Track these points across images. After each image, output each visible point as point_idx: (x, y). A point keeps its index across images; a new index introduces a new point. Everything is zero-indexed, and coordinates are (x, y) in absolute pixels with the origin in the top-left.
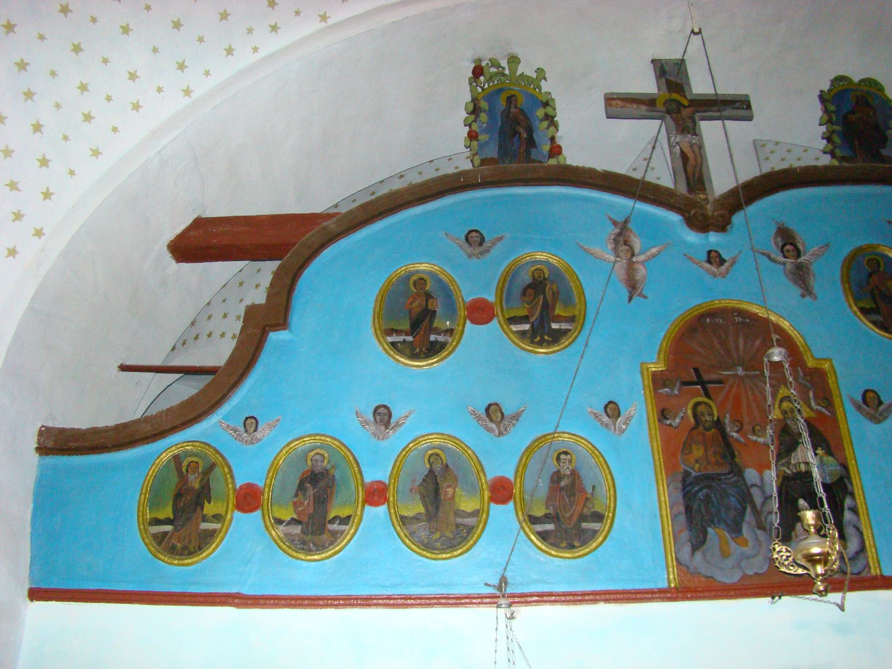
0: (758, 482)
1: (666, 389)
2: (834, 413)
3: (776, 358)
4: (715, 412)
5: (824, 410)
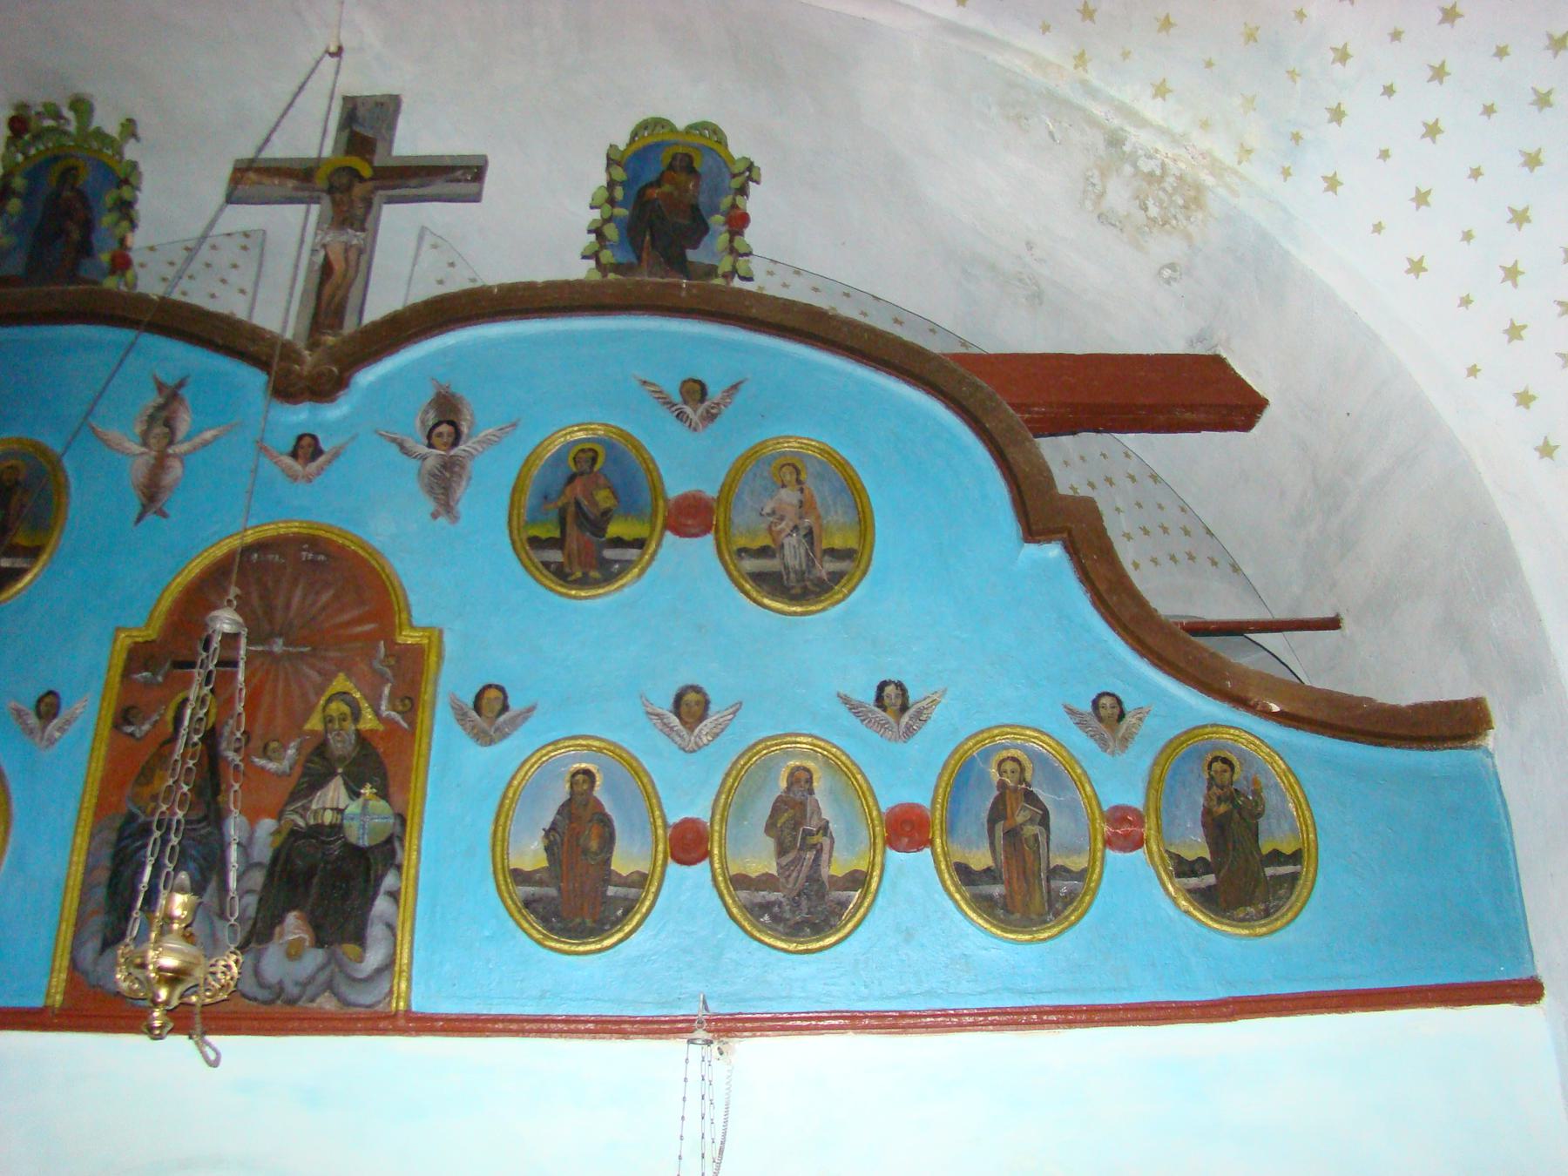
1: (144, 674)
3: (227, 628)
5: (398, 717)
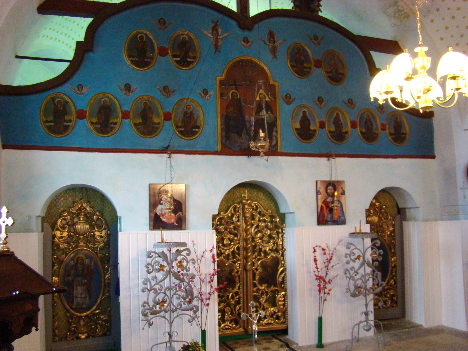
0: (248, 120)
2: (275, 100)
4: (238, 96)
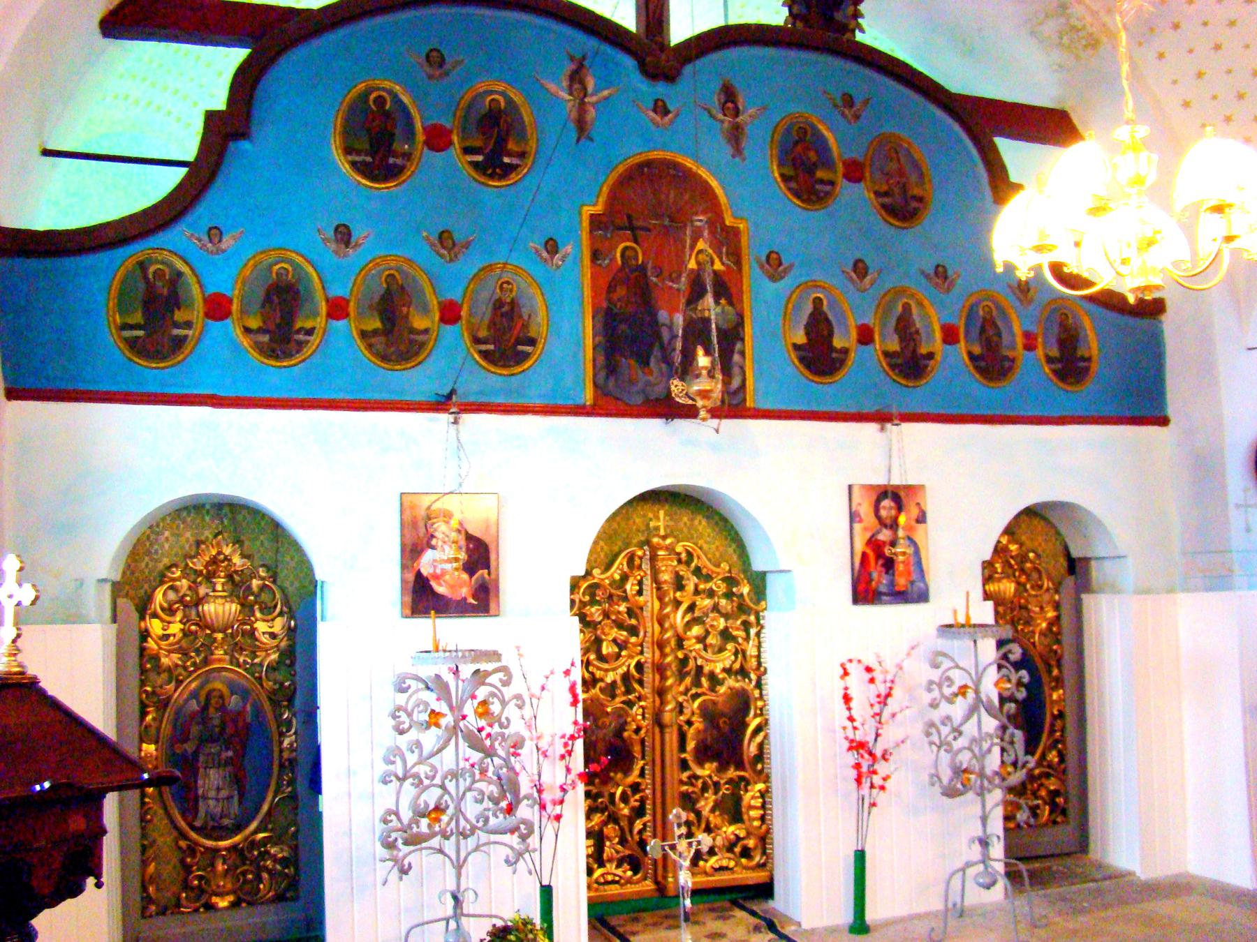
0: (667, 322)
